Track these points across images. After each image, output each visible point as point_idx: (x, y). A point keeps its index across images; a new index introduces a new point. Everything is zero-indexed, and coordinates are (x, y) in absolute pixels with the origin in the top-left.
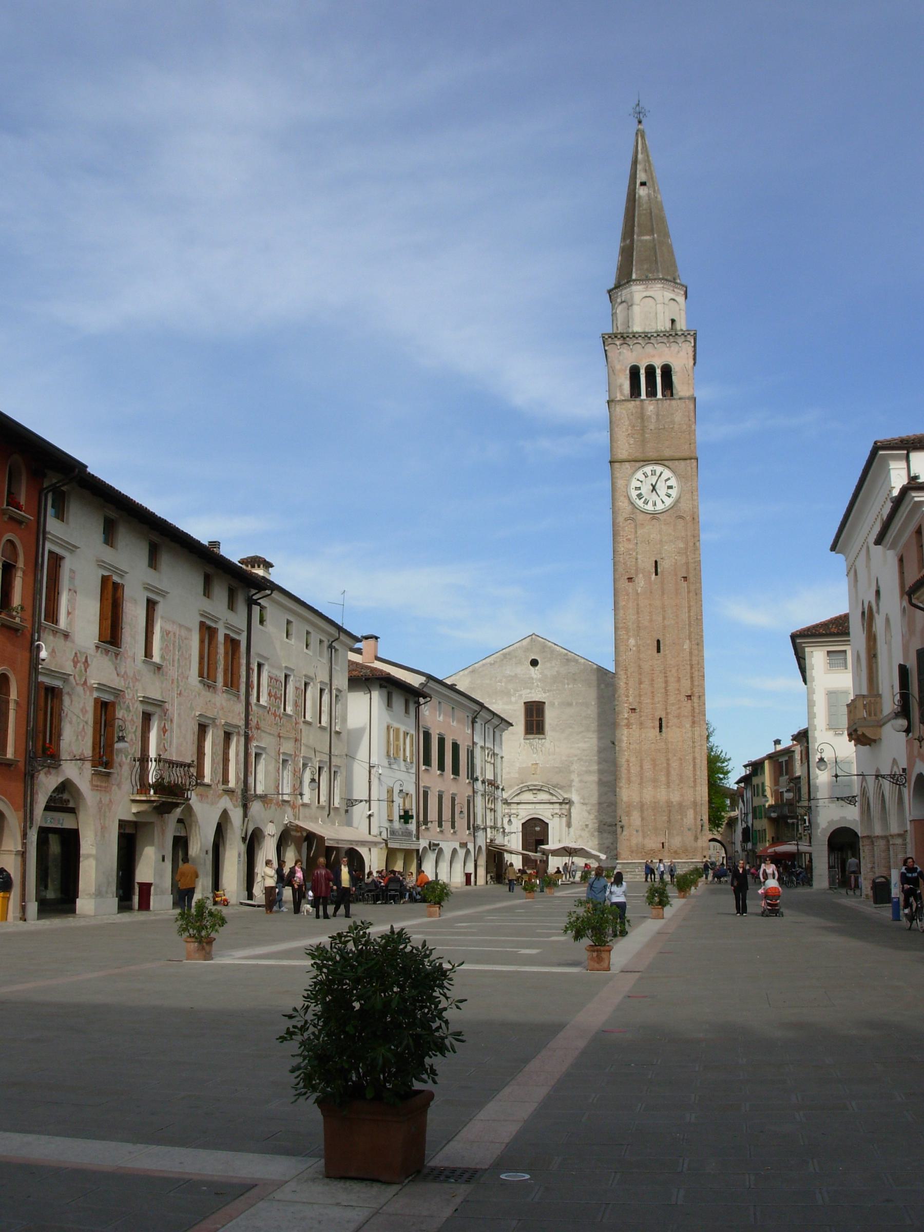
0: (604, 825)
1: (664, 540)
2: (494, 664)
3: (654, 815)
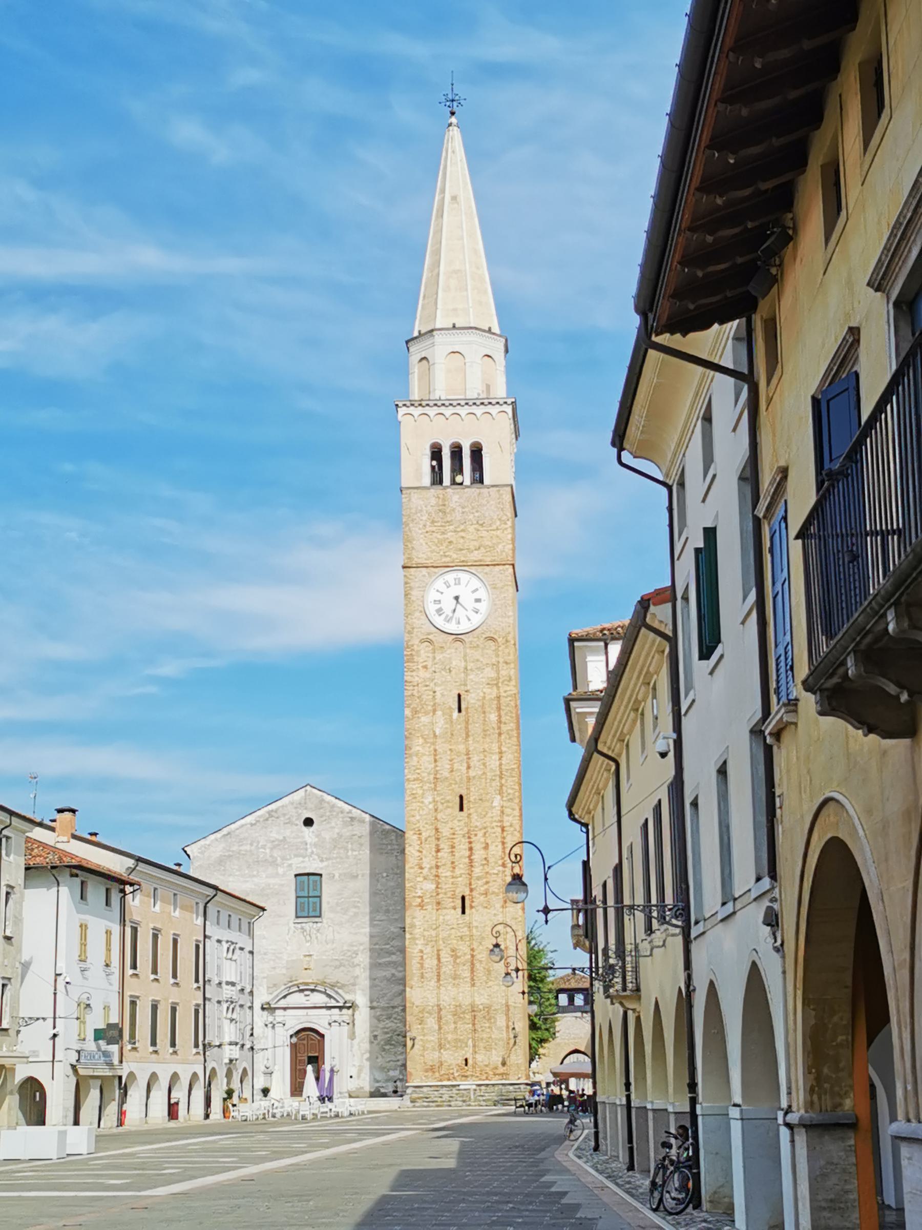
0: (398, 1035)
1: (469, 668)
2: (255, 824)
3: (455, 1023)
